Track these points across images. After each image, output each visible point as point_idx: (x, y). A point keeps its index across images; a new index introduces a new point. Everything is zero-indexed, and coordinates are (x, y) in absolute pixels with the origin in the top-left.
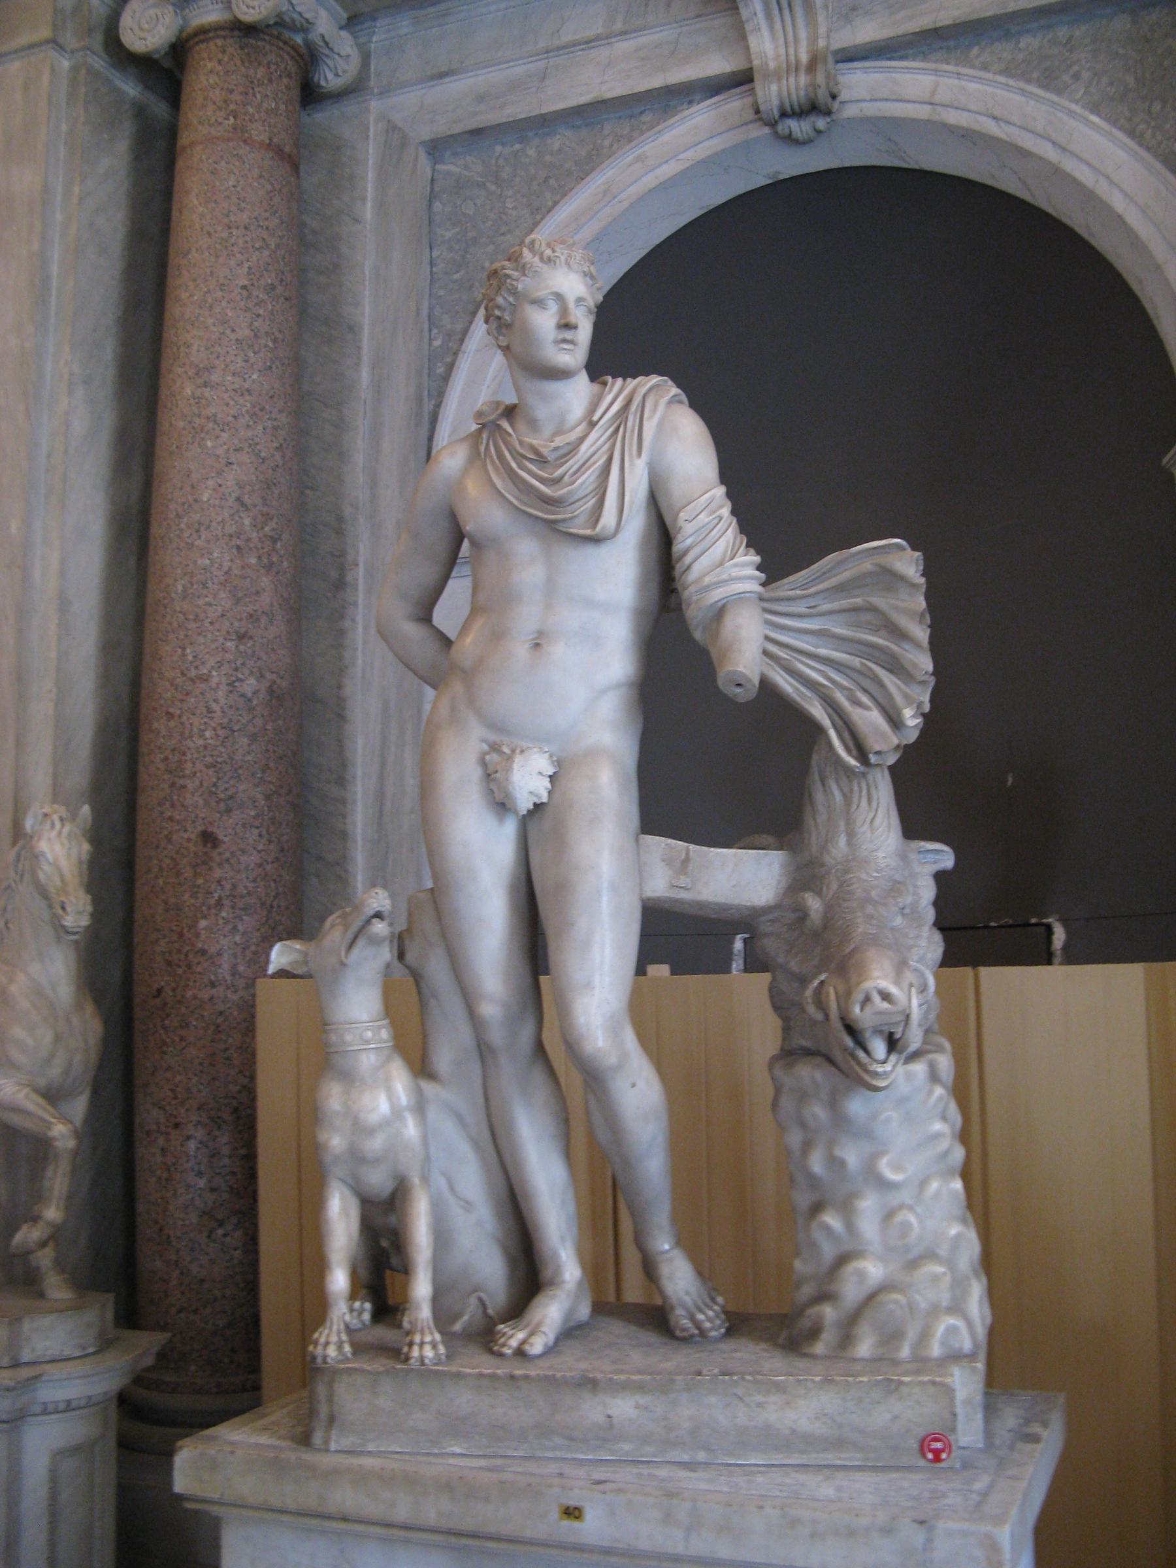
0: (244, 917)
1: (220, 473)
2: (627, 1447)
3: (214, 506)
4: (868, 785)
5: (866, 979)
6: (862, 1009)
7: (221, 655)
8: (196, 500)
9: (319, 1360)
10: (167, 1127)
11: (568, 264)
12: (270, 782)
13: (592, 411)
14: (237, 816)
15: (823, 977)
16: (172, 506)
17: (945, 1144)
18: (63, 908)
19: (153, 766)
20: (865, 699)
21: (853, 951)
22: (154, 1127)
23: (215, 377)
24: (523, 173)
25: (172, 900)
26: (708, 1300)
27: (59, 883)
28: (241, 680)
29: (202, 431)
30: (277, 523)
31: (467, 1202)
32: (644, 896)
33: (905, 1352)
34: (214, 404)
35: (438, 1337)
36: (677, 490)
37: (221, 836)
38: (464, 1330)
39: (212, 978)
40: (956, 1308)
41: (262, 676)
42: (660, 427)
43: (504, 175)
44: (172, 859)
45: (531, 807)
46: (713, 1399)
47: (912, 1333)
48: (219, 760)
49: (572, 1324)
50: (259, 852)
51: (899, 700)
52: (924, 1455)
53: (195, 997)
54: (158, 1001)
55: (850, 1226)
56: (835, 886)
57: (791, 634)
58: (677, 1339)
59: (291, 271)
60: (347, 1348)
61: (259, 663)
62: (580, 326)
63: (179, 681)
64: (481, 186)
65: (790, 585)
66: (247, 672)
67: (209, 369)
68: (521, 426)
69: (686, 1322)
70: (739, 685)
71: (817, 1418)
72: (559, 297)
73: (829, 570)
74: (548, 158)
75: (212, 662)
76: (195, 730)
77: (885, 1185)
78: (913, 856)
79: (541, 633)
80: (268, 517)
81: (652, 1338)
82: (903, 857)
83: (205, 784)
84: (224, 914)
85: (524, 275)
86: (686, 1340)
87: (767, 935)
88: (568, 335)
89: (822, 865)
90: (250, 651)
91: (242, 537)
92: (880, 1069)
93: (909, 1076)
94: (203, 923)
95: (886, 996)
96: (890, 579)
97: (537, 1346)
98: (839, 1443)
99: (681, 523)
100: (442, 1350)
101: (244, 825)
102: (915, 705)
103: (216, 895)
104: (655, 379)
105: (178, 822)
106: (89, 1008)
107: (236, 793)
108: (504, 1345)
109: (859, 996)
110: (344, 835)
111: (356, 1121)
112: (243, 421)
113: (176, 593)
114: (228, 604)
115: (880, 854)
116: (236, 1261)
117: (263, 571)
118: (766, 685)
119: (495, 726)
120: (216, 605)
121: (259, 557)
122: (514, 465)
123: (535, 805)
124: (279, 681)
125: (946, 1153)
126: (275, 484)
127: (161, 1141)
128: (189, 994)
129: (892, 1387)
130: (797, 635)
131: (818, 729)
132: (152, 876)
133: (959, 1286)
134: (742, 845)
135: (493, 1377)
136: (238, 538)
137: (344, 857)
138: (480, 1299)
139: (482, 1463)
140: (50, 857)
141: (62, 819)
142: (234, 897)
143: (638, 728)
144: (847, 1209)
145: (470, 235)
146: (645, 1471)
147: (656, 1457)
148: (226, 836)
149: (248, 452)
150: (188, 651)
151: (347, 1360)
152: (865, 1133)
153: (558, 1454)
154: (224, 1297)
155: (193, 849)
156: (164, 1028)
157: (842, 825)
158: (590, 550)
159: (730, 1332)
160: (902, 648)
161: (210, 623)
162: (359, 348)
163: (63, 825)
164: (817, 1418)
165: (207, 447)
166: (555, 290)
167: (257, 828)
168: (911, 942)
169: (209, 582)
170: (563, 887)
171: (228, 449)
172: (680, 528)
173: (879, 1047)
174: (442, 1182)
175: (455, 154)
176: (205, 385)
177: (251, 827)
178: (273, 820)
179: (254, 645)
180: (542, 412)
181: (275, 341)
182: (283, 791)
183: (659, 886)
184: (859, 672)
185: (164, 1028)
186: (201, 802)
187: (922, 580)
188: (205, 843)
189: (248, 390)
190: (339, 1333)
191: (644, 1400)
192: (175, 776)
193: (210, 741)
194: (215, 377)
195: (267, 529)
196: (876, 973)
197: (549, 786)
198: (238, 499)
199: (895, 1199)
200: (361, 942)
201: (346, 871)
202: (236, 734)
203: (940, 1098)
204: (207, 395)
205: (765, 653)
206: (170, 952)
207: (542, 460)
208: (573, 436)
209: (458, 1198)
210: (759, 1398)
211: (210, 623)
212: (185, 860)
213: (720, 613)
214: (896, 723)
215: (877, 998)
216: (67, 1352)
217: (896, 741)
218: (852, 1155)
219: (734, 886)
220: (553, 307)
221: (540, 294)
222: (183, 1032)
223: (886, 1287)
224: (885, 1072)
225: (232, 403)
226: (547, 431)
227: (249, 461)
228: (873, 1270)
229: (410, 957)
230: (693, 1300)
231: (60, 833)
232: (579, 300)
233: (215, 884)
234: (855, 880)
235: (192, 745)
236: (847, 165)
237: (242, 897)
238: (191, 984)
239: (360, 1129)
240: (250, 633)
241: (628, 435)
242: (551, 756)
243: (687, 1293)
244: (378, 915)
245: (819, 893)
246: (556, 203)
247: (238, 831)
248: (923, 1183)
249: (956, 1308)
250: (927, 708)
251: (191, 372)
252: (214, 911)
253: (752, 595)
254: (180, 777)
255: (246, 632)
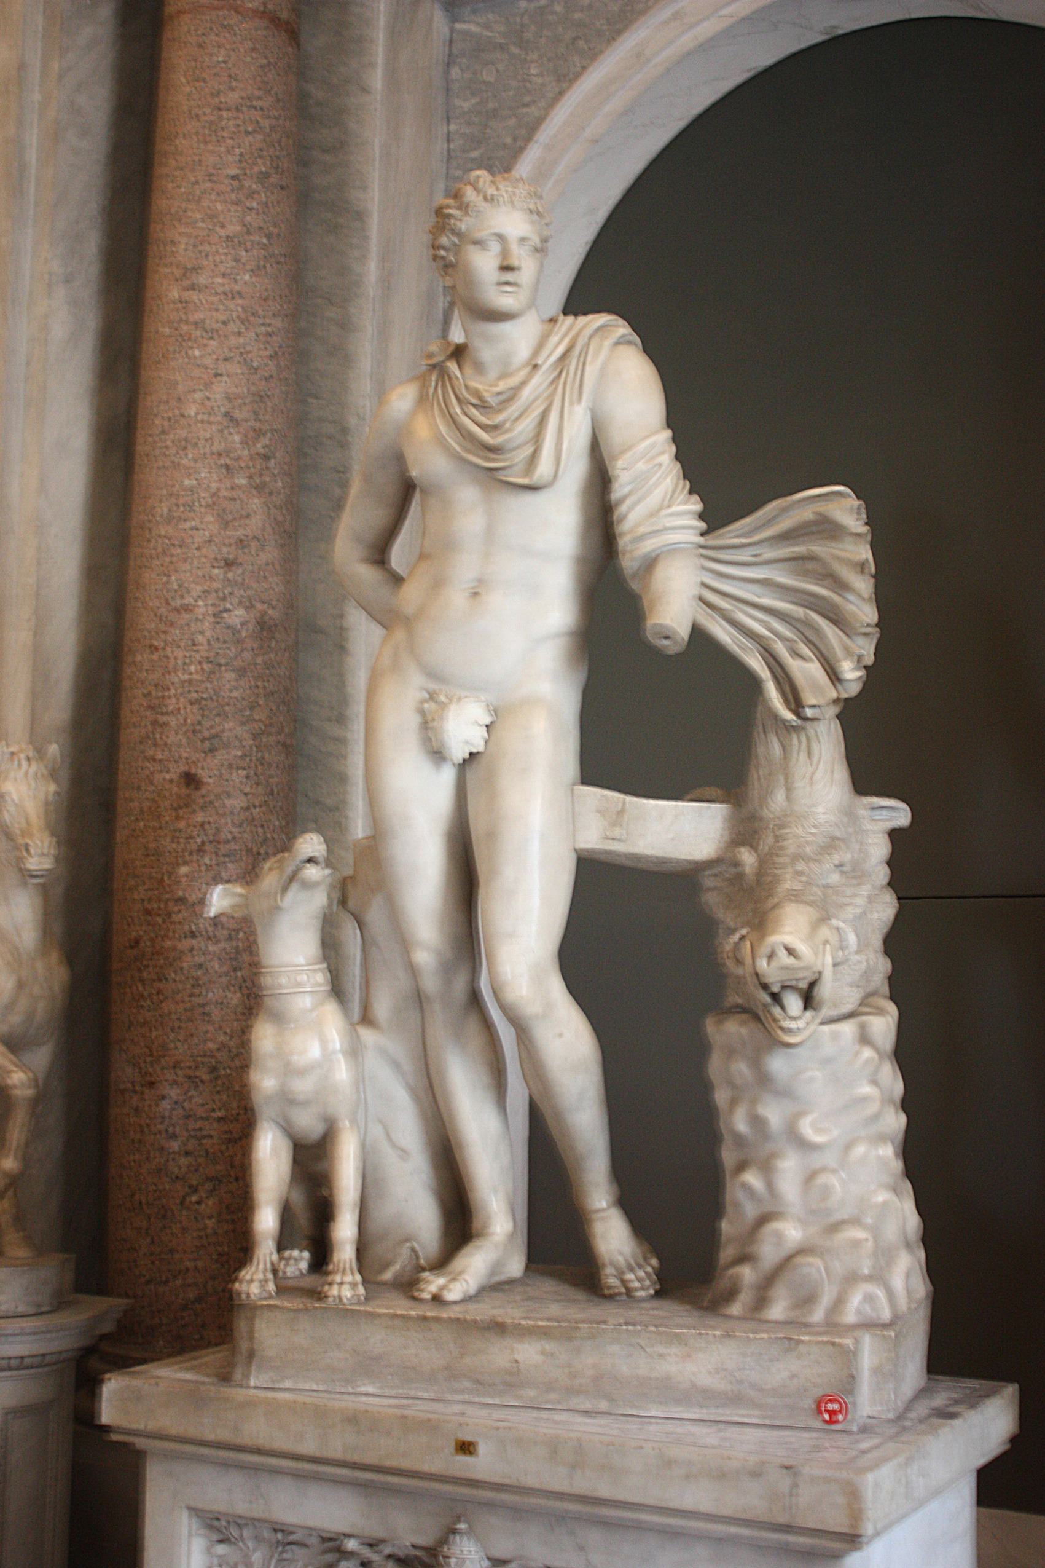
0: (229, 865)
1: (207, 385)
2: (531, 1393)
3: (202, 422)
4: (808, 739)
5: (774, 932)
6: (768, 964)
7: (208, 583)
8: (183, 416)
9: (244, 1296)
10: (142, 1086)
11: (512, 202)
12: (260, 720)
13: (537, 352)
14: (221, 756)
15: (744, 931)
16: (158, 421)
17: (873, 1108)
18: (27, 850)
19: (134, 703)
20: (806, 651)
21: (776, 906)
22: (129, 1086)
23: (202, 279)
24: (549, 34)
25: (152, 845)
26: (641, 1261)
27: (24, 825)
28: (227, 610)
29: (190, 339)
30: (270, 440)
31: (404, 1151)
32: (582, 845)
33: (818, 1315)
34: (202, 308)
35: (358, 1278)
36: (616, 437)
37: (206, 780)
38: (396, 1277)
39: (193, 928)
40: (879, 1277)
41: (252, 606)
42: (603, 372)
43: (528, 36)
44: (153, 800)
45: (467, 756)
46: (615, 1348)
47: (826, 1299)
48: (205, 696)
49: (502, 1277)
50: (246, 794)
51: (839, 652)
52: (820, 1412)
53: (174, 948)
54: (135, 952)
55: (770, 1185)
56: (770, 840)
57: (736, 583)
58: (605, 1297)
59: (289, 154)
60: (271, 1287)
61: (249, 592)
62: (523, 265)
63: (163, 611)
64: (502, 47)
65: (732, 533)
66: (235, 601)
67: (196, 269)
68: (468, 370)
69: (613, 1281)
70: (667, 638)
71: (718, 1373)
72: (501, 238)
73: (775, 517)
74: (577, 16)
75: (197, 590)
76: (180, 662)
77: (804, 1145)
78: (863, 812)
79: (480, 581)
80: (259, 433)
81: (580, 1295)
82: (850, 814)
83: (189, 722)
84: (207, 860)
85: (467, 214)
86: (611, 1297)
87: (708, 889)
88: (509, 277)
89: (761, 819)
90: (239, 579)
91: (232, 455)
92: (792, 1025)
93: (835, 1036)
94: (184, 870)
95: (790, 951)
96: (825, 528)
97: (454, 1293)
98: (735, 1399)
99: (617, 472)
100: (361, 1290)
101: (230, 766)
102: (856, 658)
103: (199, 840)
104: (602, 319)
105: (160, 761)
106: (55, 956)
107: (223, 731)
108: (422, 1291)
109: (764, 950)
110: (343, 779)
111: (288, 1064)
112: (233, 327)
113: (162, 516)
114: (214, 528)
115: (820, 810)
116: (210, 1231)
117: (254, 492)
118: (698, 633)
119: (432, 674)
120: (203, 530)
121: (251, 477)
122: (458, 410)
123: (471, 754)
124: (270, 612)
125: (876, 1117)
126: (268, 396)
127: (135, 1101)
128: (168, 943)
129: (791, 1345)
130: (742, 584)
131: (754, 684)
132: (133, 818)
133: (884, 1256)
134: (689, 797)
135: (405, 1318)
136: (228, 456)
137: (344, 802)
138: (413, 1250)
139: (392, 1401)
140: (15, 797)
141: (28, 759)
142: (219, 842)
143: (580, 678)
144: (767, 1168)
145: (491, 106)
146: (545, 1415)
147: (559, 1403)
148: (210, 777)
149: (239, 362)
150: (173, 578)
151: (270, 1297)
152: (785, 1093)
153: (466, 1397)
154: (196, 1267)
155: (175, 790)
156: (142, 981)
157: (782, 778)
158: (529, 498)
159: (659, 1294)
160: (844, 598)
161: (197, 549)
162: (366, 238)
163: (29, 766)
164: (717, 1371)
165: (195, 357)
166: (496, 231)
167: (244, 769)
168: (848, 900)
169: (197, 504)
170: (492, 835)
171: (217, 359)
172: (619, 476)
173: (793, 1003)
174: (377, 1131)
175: (475, 11)
176: (193, 287)
177: (238, 768)
178: (261, 761)
179: (243, 573)
180: (486, 353)
181: (269, 236)
182: (273, 730)
183: (592, 838)
184: (798, 620)
185: (142, 981)
186: (184, 741)
187: (865, 529)
188: (188, 785)
189: (239, 293)
190: (265, 1270)
191: (549, 1346)
192: (157, 713)
193: (195, 676)
194: (202, 279)
195: (259, 446)
196: (787, 929)
197: (486, 734)
198: (227, 414)
199: (817, 1160)
200: (294, 887)
201: (347, 818)
202: (223, 668)
203: (868, 1061)
204: (195, 298)
205: (701, 599)
206: (150, 900)
207: (483, 406)
208: (513, 381)
209: (394, 1145)
210: (661, 1349)
211: (197, 549)
212: (167, 803)
213: (650, 564)
214: (834, 676)
215: (782, 953)
216: (21, 1309)
217: (834, 695)
218: (773, 1114)
219: (673, 839)
220: (495, 247)
221: (478, 235)
222: (161, 986)
223: (803, 1251)
224: (798, 1029)
225: (221, 307)
226: (492, 375)
227: (239, 371)
228: (792, 1232)
229: (351, 903)
230: (626, 1260)
231: (26, 773)
232: (523, 240)
233: (198, 828)
234: (790, 835)
235: (176, 680)
236: (913, 16)
237: (227, 842)
238: (171, 934)
239: (289, 1070)
240: (240, 560)
241: (570, 380)
242: (488, 706)
243: (621, 1253)
244: (310, 860)
245: (754, 847)
246: (584, 68)
247: (223, 772)
248: (848, 1147)
249: (879, 1277)
250: (870, 660)
251: (178, 273)
252: (195, 857)
253: (689, 546)
254: (162, 714)
255: (236, 559)
